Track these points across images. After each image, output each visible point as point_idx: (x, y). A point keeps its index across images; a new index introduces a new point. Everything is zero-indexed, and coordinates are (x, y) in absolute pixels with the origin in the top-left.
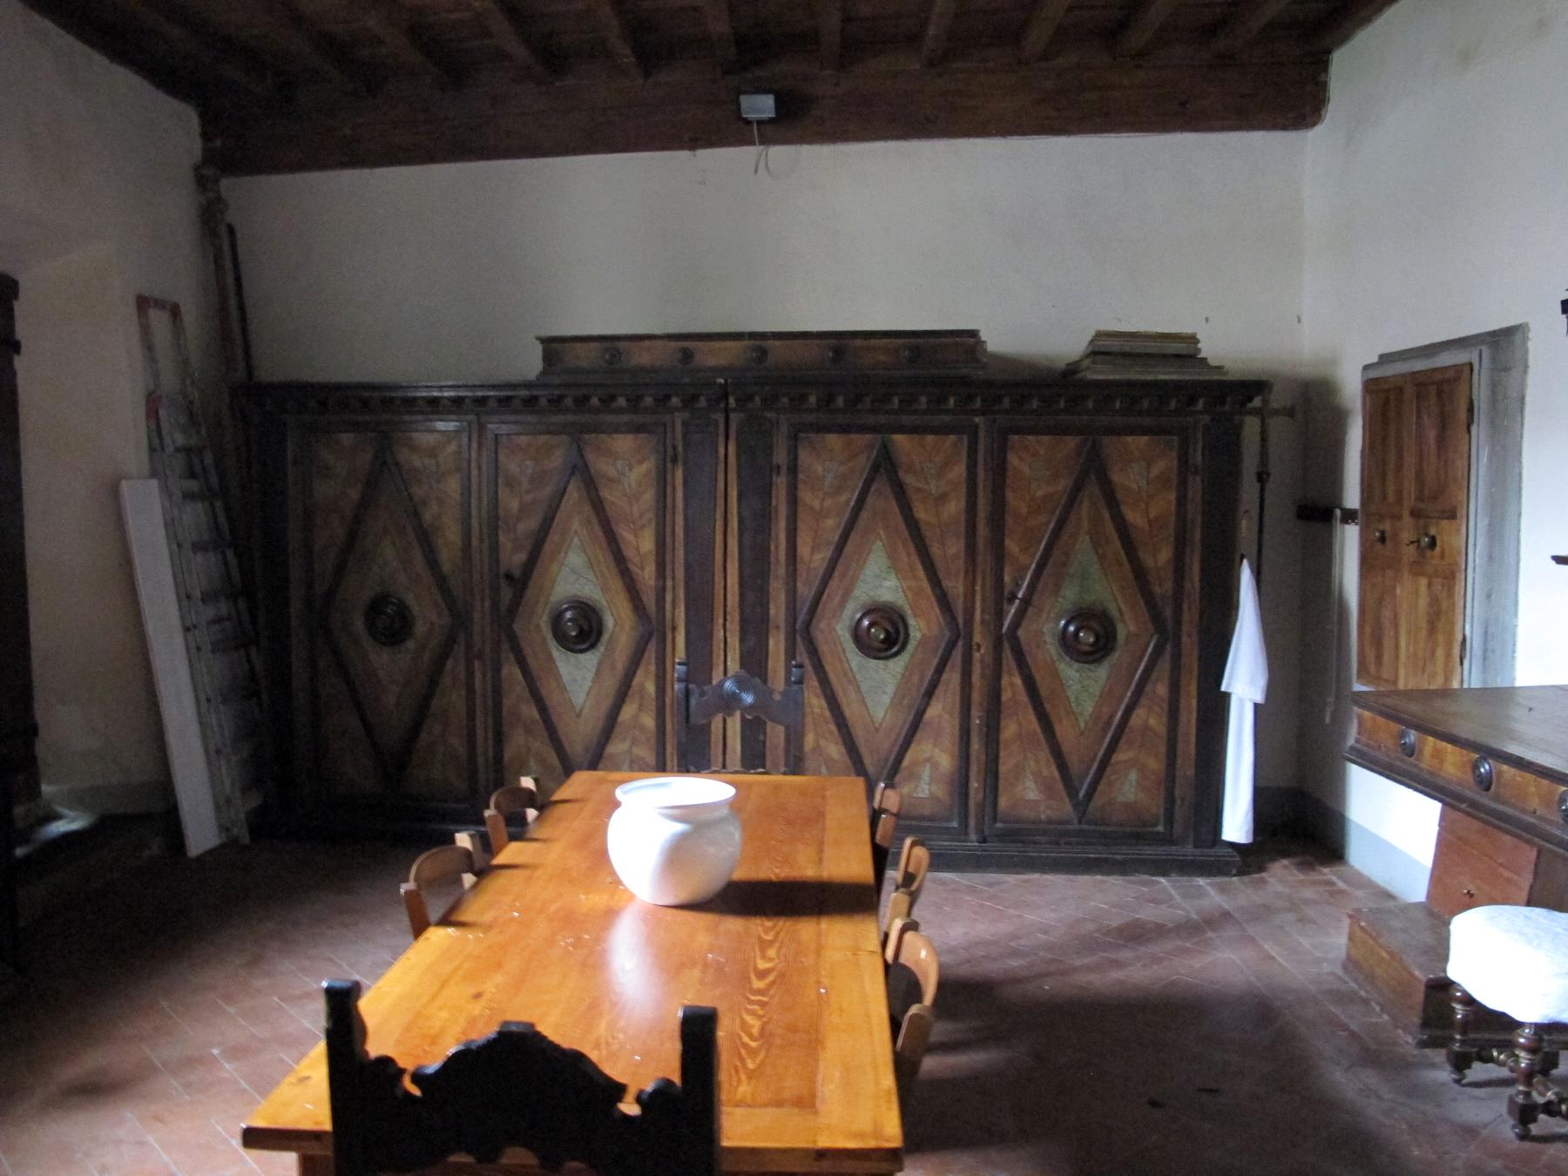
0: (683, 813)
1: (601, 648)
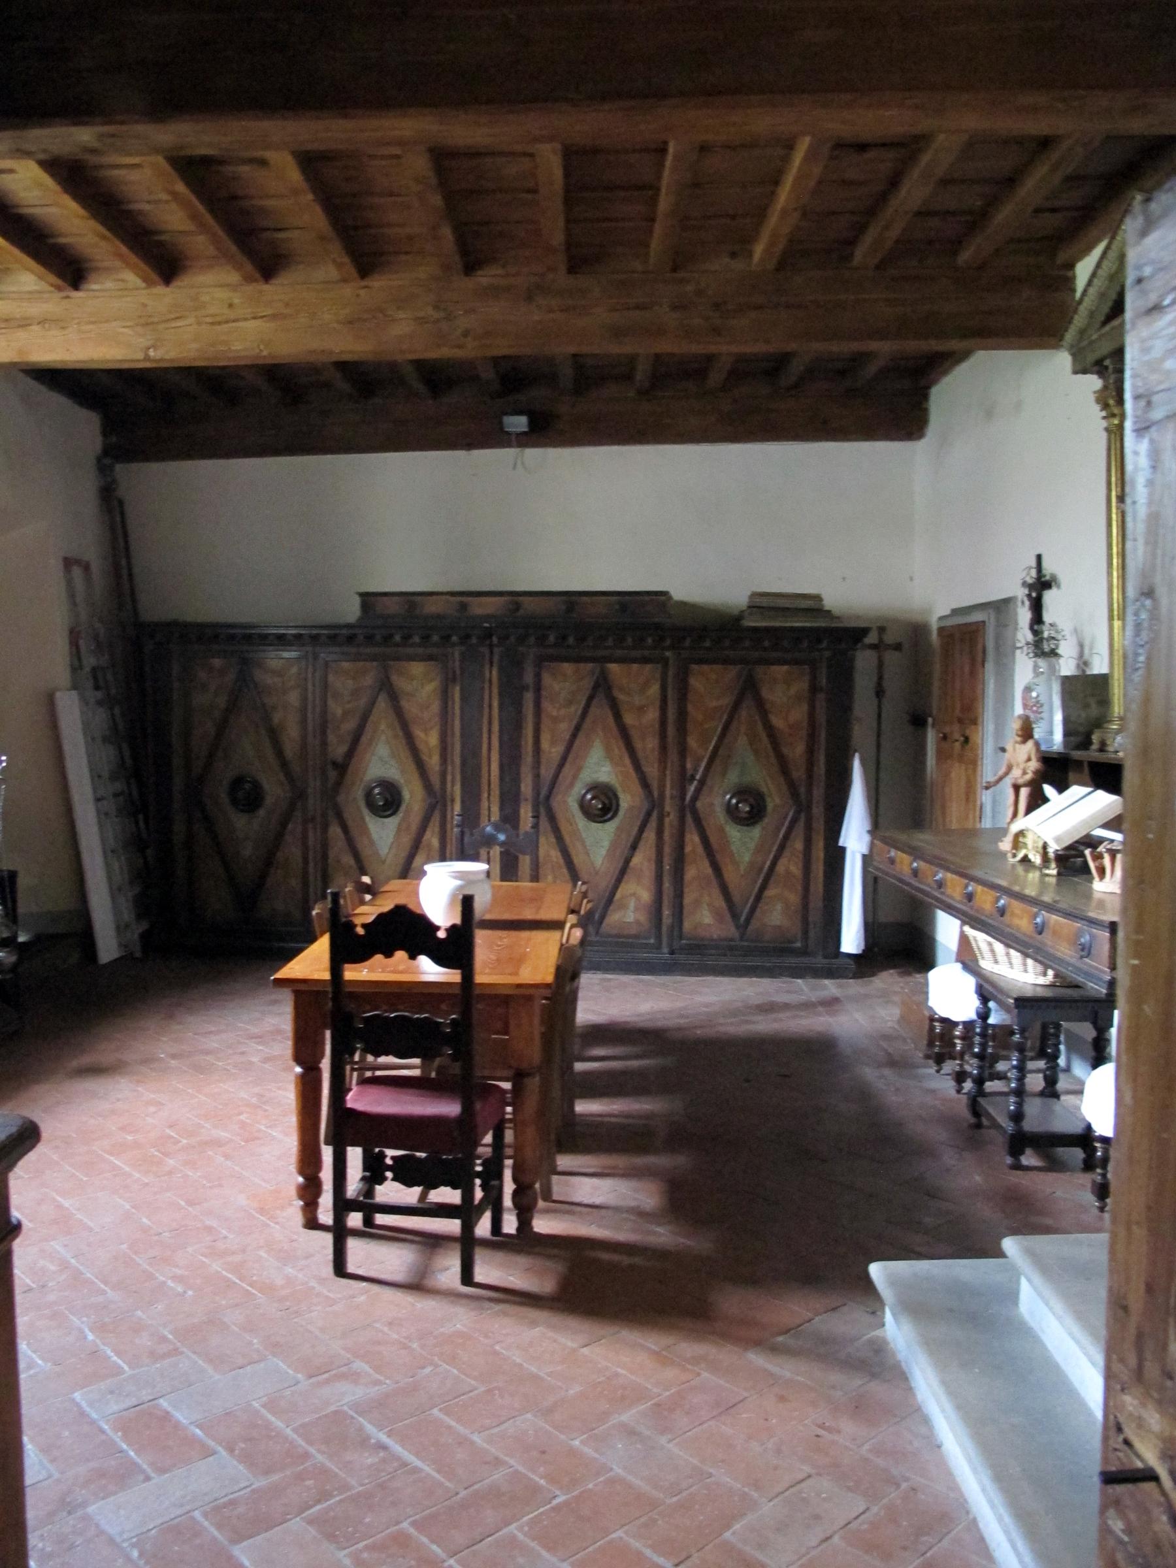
0: (460, 875)
1: (400, 814)
